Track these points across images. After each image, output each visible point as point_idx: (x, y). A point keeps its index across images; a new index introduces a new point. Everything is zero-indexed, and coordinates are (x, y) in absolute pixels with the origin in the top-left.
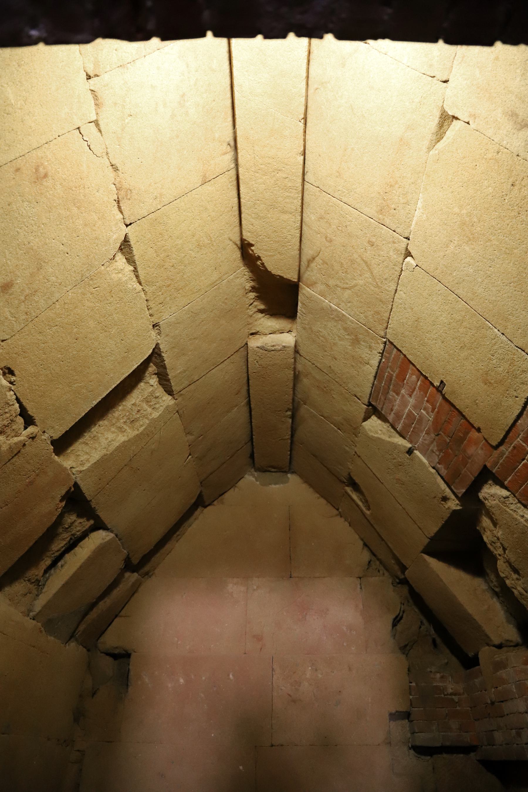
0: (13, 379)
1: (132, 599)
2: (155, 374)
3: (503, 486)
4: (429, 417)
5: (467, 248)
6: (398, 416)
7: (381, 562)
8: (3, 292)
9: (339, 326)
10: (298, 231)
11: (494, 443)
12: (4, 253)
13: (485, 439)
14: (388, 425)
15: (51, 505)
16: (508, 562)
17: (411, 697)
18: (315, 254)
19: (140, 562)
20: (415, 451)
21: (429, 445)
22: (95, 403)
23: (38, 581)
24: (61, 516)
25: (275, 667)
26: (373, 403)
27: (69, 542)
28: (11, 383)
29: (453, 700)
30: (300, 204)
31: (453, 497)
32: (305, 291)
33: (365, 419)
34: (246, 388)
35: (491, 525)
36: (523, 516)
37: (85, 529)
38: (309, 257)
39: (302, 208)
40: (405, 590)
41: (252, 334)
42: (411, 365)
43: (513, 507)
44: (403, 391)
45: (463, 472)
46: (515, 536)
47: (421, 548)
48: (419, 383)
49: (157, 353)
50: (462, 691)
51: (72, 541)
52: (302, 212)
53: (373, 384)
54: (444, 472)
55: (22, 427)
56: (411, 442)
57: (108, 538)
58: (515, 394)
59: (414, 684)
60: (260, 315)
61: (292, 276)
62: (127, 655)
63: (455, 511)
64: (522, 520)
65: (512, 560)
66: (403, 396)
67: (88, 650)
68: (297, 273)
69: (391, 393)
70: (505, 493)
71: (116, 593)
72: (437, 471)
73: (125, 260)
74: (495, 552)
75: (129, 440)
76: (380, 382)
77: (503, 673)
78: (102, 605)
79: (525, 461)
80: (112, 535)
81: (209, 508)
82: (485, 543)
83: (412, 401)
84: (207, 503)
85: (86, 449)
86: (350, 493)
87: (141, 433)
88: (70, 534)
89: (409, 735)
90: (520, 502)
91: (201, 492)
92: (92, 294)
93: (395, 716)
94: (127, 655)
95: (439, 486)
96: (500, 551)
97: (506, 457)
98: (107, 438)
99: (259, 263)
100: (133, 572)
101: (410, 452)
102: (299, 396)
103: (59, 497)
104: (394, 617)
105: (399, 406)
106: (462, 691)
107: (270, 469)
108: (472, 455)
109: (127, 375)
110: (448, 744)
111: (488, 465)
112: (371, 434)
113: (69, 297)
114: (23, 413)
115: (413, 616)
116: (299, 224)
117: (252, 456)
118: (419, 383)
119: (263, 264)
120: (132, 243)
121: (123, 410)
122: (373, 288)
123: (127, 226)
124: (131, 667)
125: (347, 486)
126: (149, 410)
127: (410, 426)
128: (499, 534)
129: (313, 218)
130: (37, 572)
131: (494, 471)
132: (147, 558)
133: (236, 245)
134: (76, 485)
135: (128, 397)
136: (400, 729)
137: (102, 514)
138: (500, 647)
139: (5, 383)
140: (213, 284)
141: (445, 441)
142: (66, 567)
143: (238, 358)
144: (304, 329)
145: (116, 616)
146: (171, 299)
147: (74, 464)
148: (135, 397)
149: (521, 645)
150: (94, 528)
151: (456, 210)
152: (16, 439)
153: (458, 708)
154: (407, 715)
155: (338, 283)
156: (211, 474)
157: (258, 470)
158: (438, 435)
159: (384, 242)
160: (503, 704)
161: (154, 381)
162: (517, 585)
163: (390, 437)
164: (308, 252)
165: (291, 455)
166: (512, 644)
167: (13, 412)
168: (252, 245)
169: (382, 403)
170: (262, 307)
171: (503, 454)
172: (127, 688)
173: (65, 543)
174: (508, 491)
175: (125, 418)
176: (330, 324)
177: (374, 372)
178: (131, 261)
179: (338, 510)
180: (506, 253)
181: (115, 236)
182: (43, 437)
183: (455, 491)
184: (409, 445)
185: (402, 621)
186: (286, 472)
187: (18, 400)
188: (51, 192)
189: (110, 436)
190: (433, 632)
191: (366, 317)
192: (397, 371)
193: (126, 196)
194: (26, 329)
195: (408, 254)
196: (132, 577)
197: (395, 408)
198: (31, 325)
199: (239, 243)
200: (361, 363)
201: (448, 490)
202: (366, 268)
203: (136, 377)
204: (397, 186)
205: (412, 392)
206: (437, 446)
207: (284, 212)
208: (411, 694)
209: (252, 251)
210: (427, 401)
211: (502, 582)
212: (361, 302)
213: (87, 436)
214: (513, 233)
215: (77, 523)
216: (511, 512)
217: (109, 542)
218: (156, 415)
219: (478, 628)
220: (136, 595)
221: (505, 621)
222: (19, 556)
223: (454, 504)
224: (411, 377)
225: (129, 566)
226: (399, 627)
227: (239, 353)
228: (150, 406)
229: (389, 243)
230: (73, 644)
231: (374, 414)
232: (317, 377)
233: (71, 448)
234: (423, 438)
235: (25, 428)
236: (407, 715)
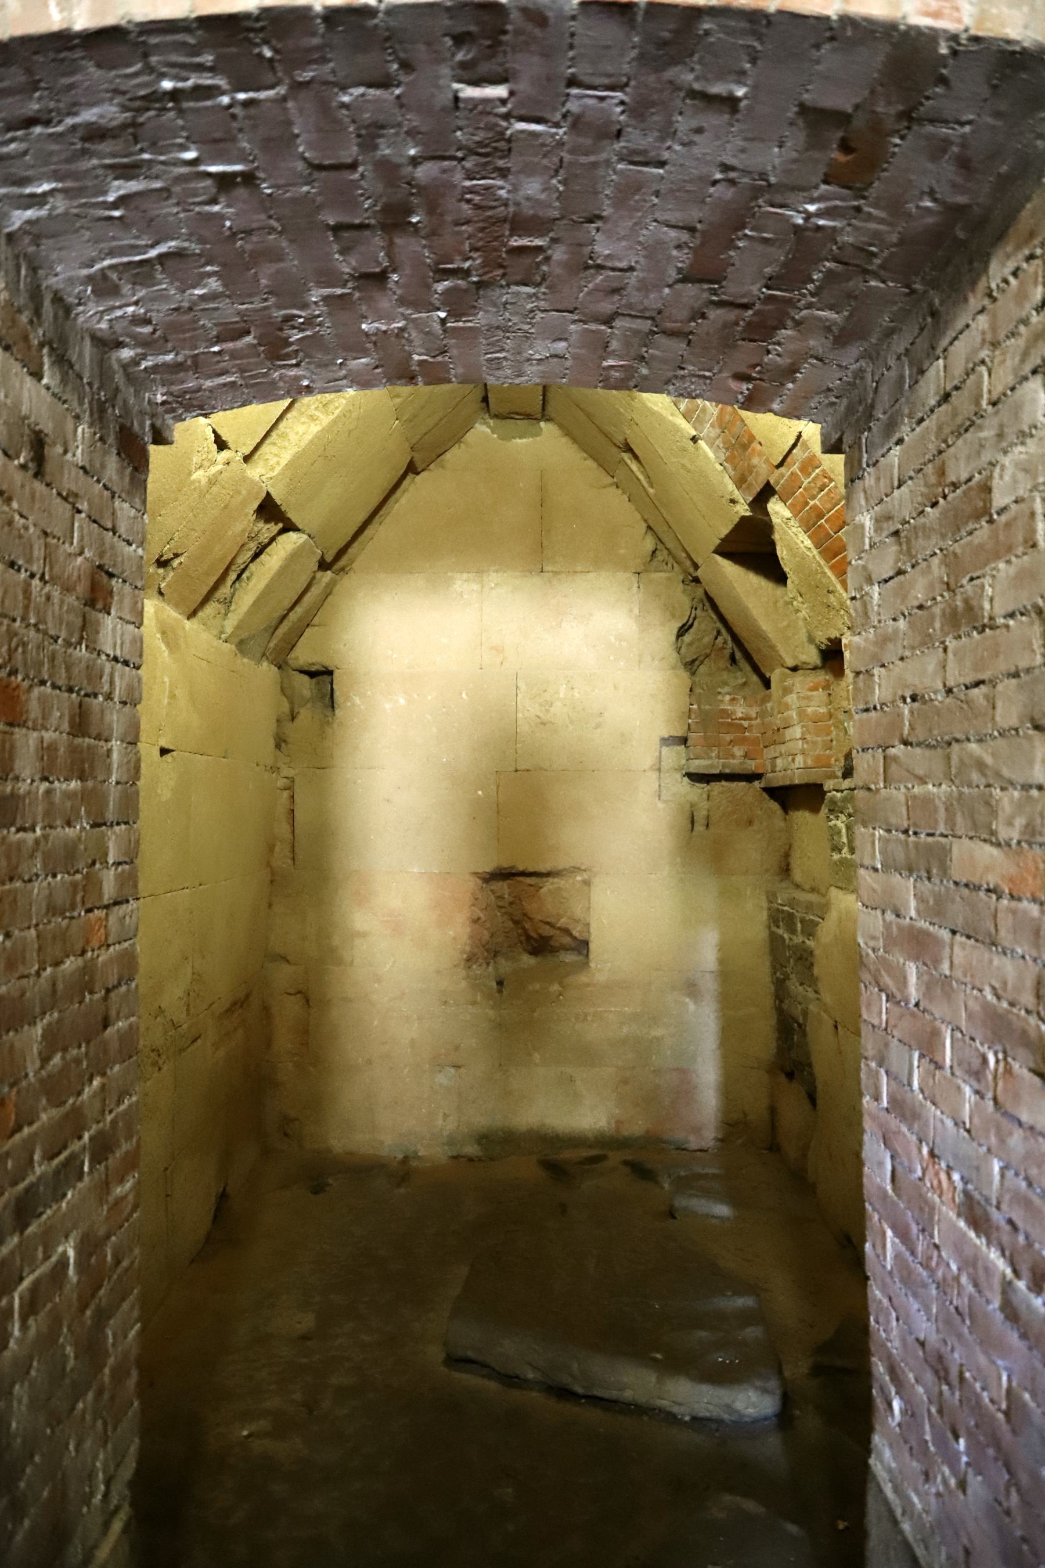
7: (670, 552)
47: (713, 548)
57: (301, 541)
62: (330, 673)
63: (743, 518)
67: (279, 668)
78: (293, 616)
81: (423, 474)
85: (274, 450)
87: (338, 417)
89: (684, 762)
93: (666, 741)
110: (727, 771)
111: (772, 482)
115: (706, 624)
130: (225, 591)
136: (673, 756)
137: (293, 516)
147: (263, 472)
150: (282, 531)
154: (684, 741)
157: (496, 416)
171: (783, 476)
184: (694, 433)
185: (692, 630)
186: (538, 420)
189: (301, 429)
217: (302, 546)
223: (743, 509)
225: (324, 565)
226: (687, 638)
236: (684, 741)
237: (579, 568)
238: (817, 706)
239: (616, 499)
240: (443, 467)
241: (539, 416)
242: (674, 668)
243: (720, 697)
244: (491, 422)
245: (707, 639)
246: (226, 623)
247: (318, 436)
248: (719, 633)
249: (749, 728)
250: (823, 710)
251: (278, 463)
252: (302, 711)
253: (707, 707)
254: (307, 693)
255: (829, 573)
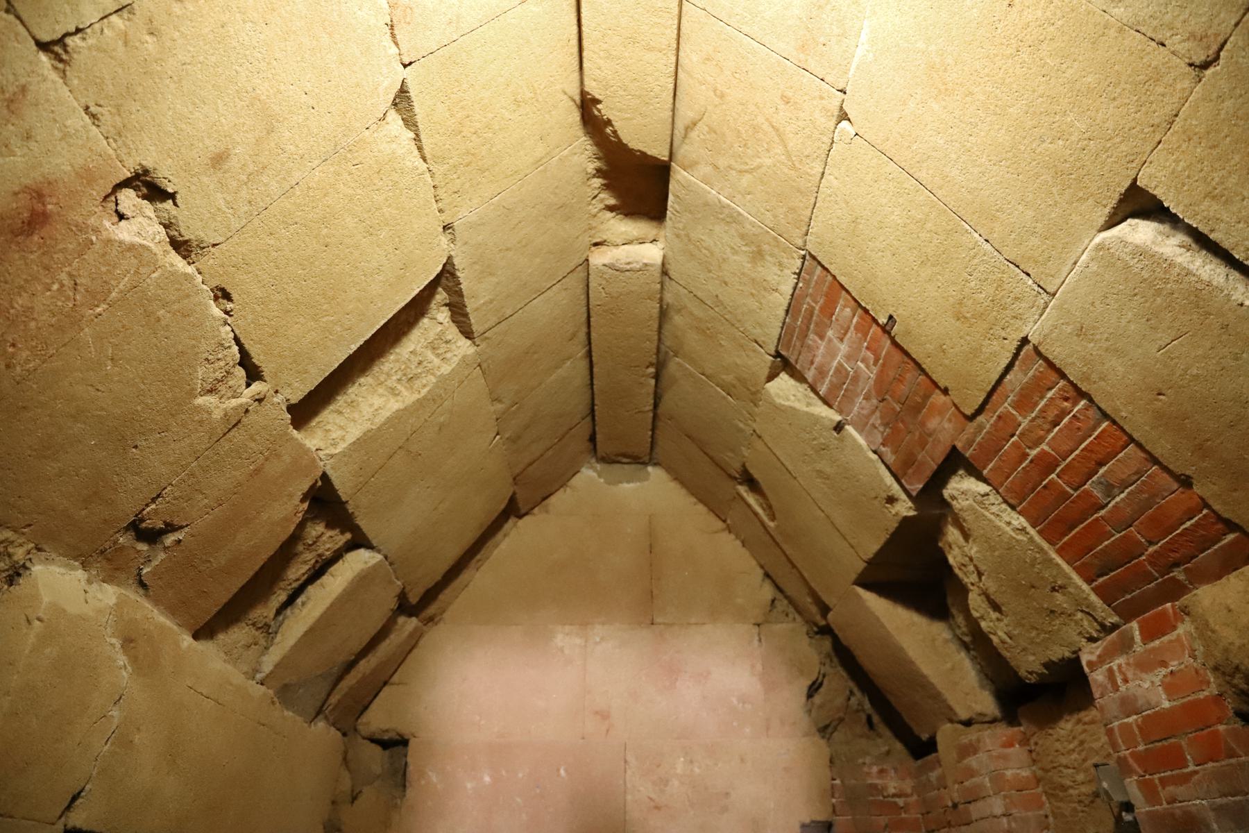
0: (229, 306)
1: (410, 656)
2: (446, 305)
3: (981, 478)
4: (869, 373)
5: (936, 107)
6: (822, 373)
7: (791, 601)
8: (214, 167)
9: (733, 232)
10: (671, 80)
11: (969, 412)
12: (216, 104)
13: (955, 405)
14: (806, 386)
15: (288, 507)
16: (985, 594)
17: (834, 800)
18: (698, 117)
19: (420, 603)
20: (847, 427)
21: (868, 417)
22: (354, 347)
23: (267, 626)
24: (301, 526)
25: (629, 758)
26: (783, 353)
27: (314, 566)
28: (227, 313)
29: (895, 803)
30: (675, 36)
31: (903, 496)
32: (680, 177)
33: (771, 378)
34: (584, 329)
35: (961, 539)
36: (1009, 523)
37: (337, 546)
38: (687, 122)
39: (678, 43)
40: (827, 644)
41: (596, 244)
42: (844, 292)
43: (994, 509)
44: (830, 333)
45: (920, 457)
46: (997, 553)
47: (854, 576)
48: (855, 320)
49: (448, 272)
50: (909, 791)
51: (318, 566)
52: (678, 49)
53: (784, 323)
54: (890, 458)
55: (243, 382)
56: (840, 412)
57: (373, 562)
58: (1004, 335)
59: (838, 782)
60: (609, 215)
61: (661, 153)
62: (403, 742)
63: (906, 518)
64: (1008, 529)
65: (992, 590)
66: (830, 340)
67: (344, 734)
68: (668, 146)
69: (812, 336)
70: (983, 488)
71: (385, 648)
72: (880, 457)
73: (401, 122)
74: (966, 580)
75: (406, 409)
76: (795, 319)
77: (972, 761)
78: (365, 666)
79: (1015, 438)
80: (379, 557)
81: (526, 518)
82: (950, 568)
83: (844, 348)
84: (523, 511)
85: (340, 420)
86: (745, 495)
87: (424, 398)
88: (314, 554)
90: (1005, 501)
91: (514, 493)
92: (350, 174)
94: (403, 742)
95: (882, 480)
96: (974, 578)
97: (988, 433)
98: (370, 405)
99: (608, 130)
100: (410, 615)
101: (839, 427)
102: (668, 343)
103: (299, 495)
104: (810, 682)
105: (823, 356)
106: (909, 791)
107: (620, 458)
108: (935, 430)
109: (403, 304)
111: (959, 445)
112: (779, 401)
113: (316, 179)
114: (245, 360)
115: (838, 682)
116: (673, 69)
117: (592, 438)
118: (855, 320)
119: (615, 132)
120: (412, 94)
121: (397, 361)
122: (786, 170)
123: (405, 66)
124: (409, 760)
125: (740, 484)
126: (437, 361)
127: (840, 388)
128: (973, 552)
129: (695, 59)
130: (265, 612)
131: (967, 455)
132: (431, 595)
133: (574, 101)
134: (325, 477)
135: (405, 340)
137: (362, 522)
138: (968, 723)
139: (216, 312)
140: (538, 162)
141: (893, 409)
142: (309, 606)
143: (575, 282)
144: (678, 236)
145: (385, 683)
146: (472, 186)
147: (322, 445)
148: (414, 342)
149: (1000, 721)
150: (352, 546)
151: (921, 45)
152: (234, 402)
153: (903, 815)
155: (732, 162)
156: (530, 464)
157: (605, 460)
158: (883, 400)
159: (806, 98)
160: (972, 807)
161: (443, 315)
162: (997, 628)
163: (808, 405)
164: (686, 113)
165: (652, 437)
166: (987, 719)
167: (229, 359)
168: (599, 102)
169: (796, 353)
170: (612, 202)
172: (404, 791)
173: (307, 567)
174: (989, 484)
175: (400, 373)
176: (718, 229)
177: (785, 303)
178: (410, 123)
179: (724, 521)
180: (996, 114)
181: (386, 84)
182: (275, 400)
183: (908, 487)
184: (838, 418)
185: (822, 690)
186: (645, 464)
187: (237, 339)
188: (288, 8)
189: (377, 402)
190: (867, 706)
191: (775, 216)
192: (822, 301)
193: (405, 17)
194: (250, 226)
195: (843, 116)
196: (408, 624)
197: (818, 360)
198: (256, 222)
199: (578, 98)
200: (765, 289)
201: (896, 486)
202: (776, 139)
203: (416, 309)
204: (829, 7)
205: (845, 334)
206: (882, 418)
207: (650, 49)
208: (833, 796)
209: (599, 111)
210: (867, 348)
211: (974, 625)
212: (767, 193)
213: (341, 400)
214: (1007, 81)
215: (327, 538)
216: (992, 517)
218: (446, 369)
219: (936, 696)
220: (415, 651)
221: (976, 685)
222: (240, 586)
223: (905, 508)
224: (843, 311)
225: (405, 607)
226: (817, 699)
227: (575, 274)
228: (438, 355)
229: (814, 98)
230: (321, 724)
231: (783, 370)
232: (696, 313)
233: (317, 419)
234: (859, 405)
235: (248, 385)
237: (693, 620)
238: (1017, 767)
239: (729, 545)
240: (547, 512)
241: (646, 459)
242: (806, 735)
243: (866, 769)
244: (598, 466)
245: (840, 701)
246: (265, 658)
247: (399, 416)
248: (852, 693)
249: (905, 808)
250: (1025, 773)
251: (343, 439)
252: (366, 790)
253: (853, 782)
254: (377, 769)
255: (1059, 560)
